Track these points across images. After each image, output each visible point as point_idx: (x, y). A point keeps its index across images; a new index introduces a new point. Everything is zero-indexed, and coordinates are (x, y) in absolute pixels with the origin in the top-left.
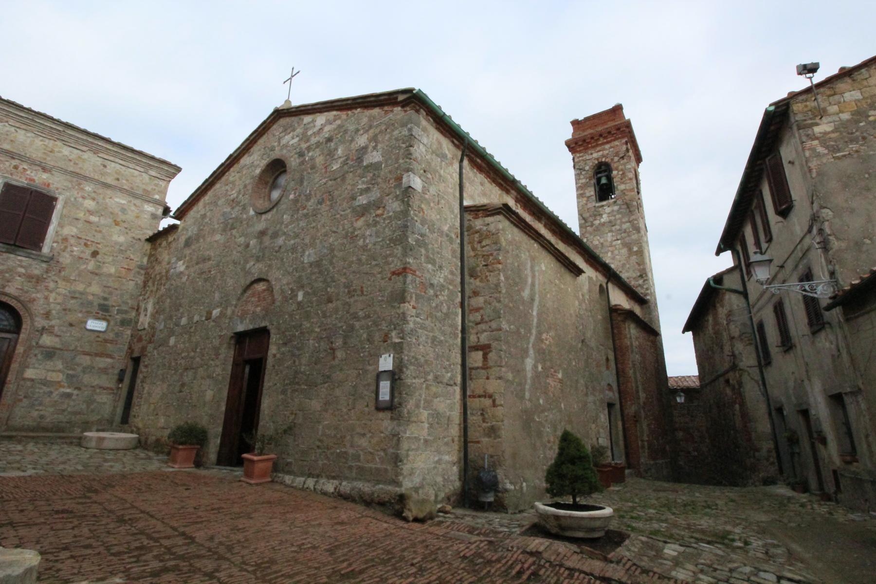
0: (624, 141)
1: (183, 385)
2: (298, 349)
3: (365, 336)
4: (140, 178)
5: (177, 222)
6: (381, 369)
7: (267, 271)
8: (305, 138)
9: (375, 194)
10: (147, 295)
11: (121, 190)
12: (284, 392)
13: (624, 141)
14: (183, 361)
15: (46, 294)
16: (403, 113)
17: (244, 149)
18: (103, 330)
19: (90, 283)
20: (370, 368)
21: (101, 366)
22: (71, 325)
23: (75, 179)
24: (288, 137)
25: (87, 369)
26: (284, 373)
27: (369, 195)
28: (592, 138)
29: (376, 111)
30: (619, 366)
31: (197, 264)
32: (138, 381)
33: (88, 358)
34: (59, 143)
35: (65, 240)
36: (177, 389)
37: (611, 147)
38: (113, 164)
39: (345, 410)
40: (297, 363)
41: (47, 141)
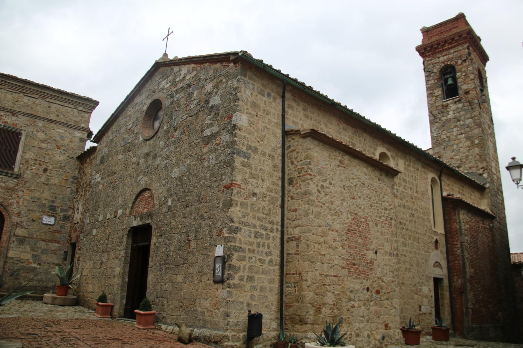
0: (466, 46)
1: (102, 263)
2: (169, 240)
3: (208, 231)
4: (71, 114)
5: (96, 145)
6: (217, 255)
7: (150, 183)
8: (174, 83)
9: (215, 129)
10: (79, 198)
11: (61, 123)
12: (161, 270)
13: (466, 46)
14: (101, 246)
15: (18, 199)
16: (234, 68)
17: (136, 91)
18: (52, 223)
19: (43, 191)
20: (211, 254)
21: (53, 249)
22: (33, 221)
23: (32, 119)
24: (164, 83)
25: (45, 251)
26: (161, 256)
27: (212, 128)
28: (438, 44)
29: (218, 65)
30: (449, 246)
31: (108, 176)
32: (76, 260)
33: (44, 243)
34: (21, 95)
35: (27, 162)
36: (98, 266)
37: (455, 52)
38: (55, 105)
39: (196, 282)
40: (168, 250)
41: (14, 94)
